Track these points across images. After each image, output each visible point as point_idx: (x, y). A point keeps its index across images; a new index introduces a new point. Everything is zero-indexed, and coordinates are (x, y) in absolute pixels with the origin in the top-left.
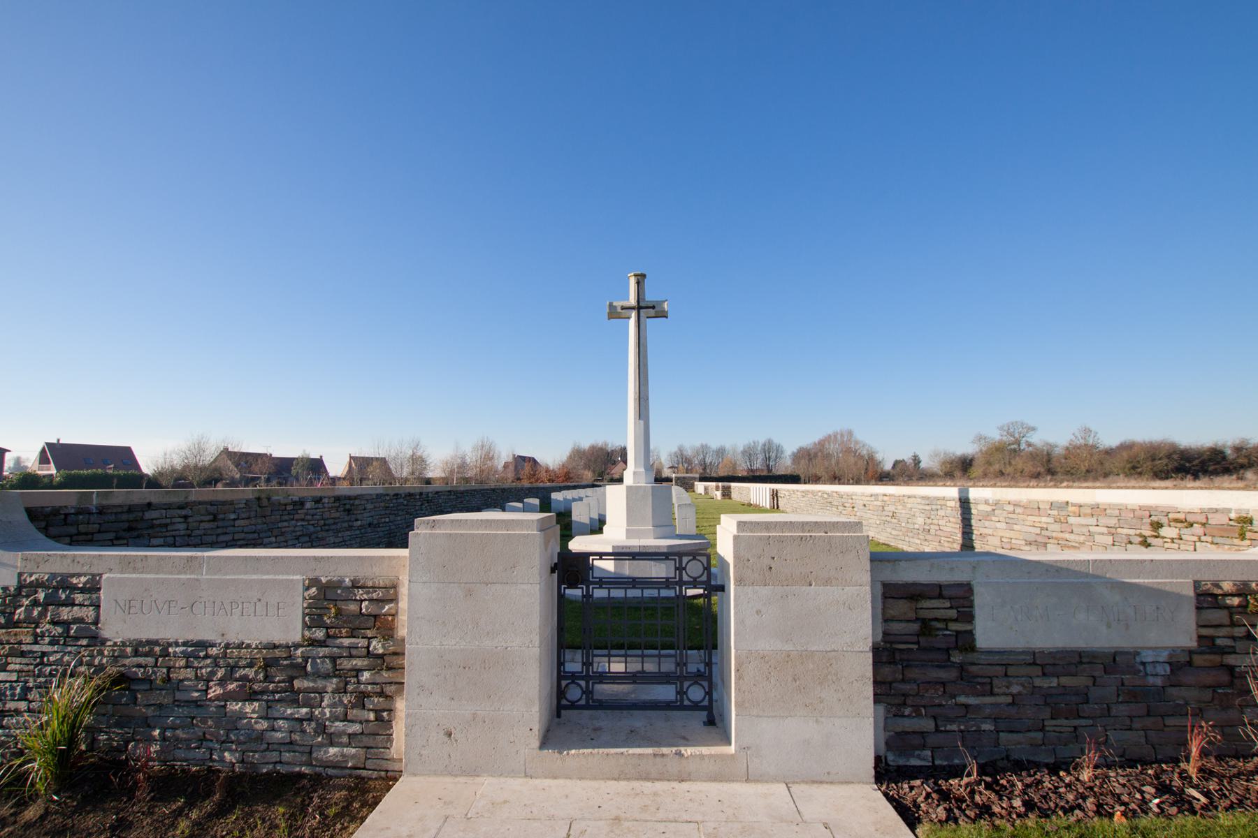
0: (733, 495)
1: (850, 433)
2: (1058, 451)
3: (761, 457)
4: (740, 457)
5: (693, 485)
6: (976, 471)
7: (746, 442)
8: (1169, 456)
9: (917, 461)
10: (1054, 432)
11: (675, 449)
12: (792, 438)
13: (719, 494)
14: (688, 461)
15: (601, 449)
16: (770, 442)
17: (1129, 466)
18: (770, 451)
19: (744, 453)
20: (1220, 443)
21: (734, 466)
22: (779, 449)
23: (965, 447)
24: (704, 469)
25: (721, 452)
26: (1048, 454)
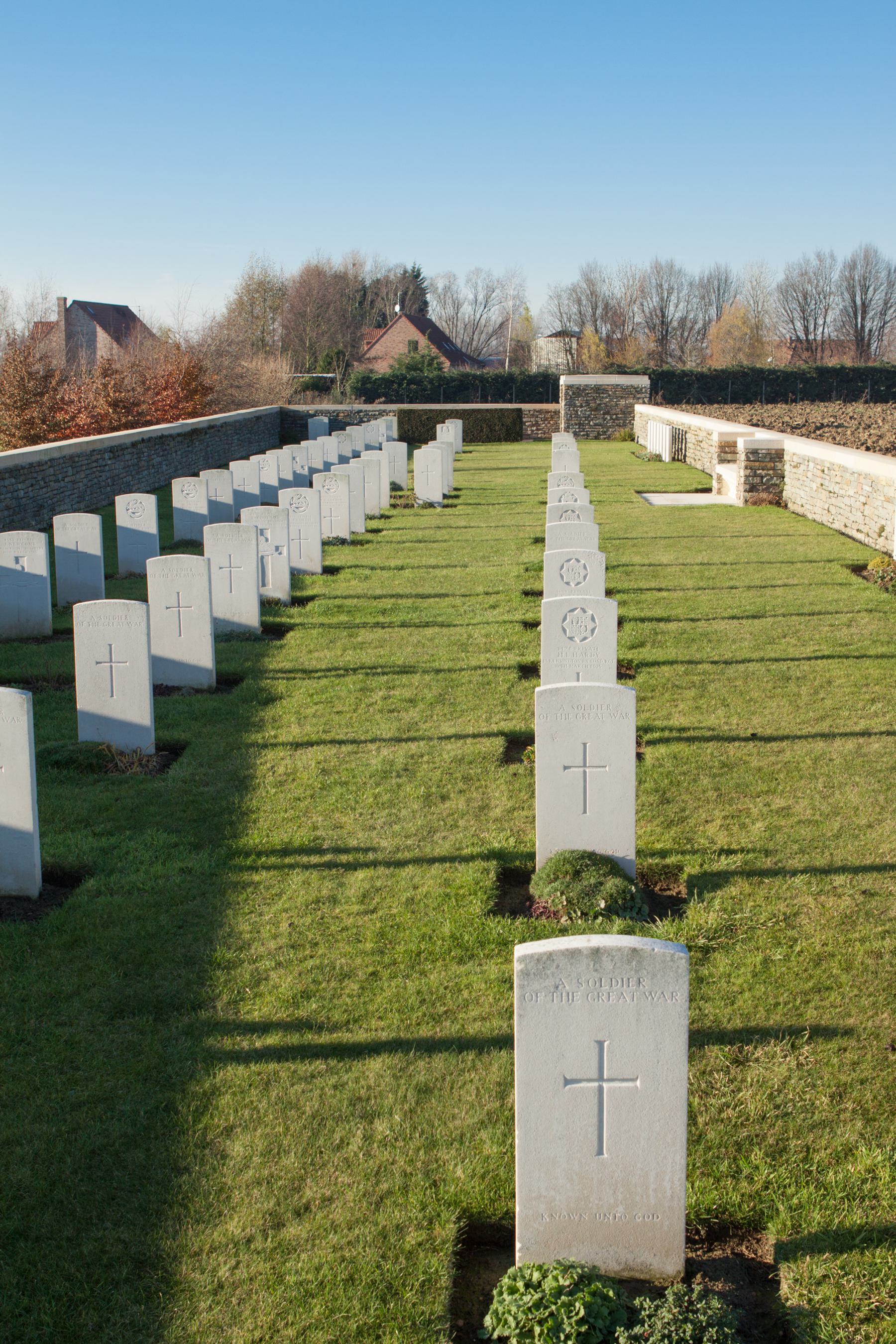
0: (791, 491)
3: (838, 304)
4: (773, 303)
5: (629, 413)
11: (571, 277)
13: (731, 482)
14: (613, 314)
15: (340, 278)
16: (869, 257)
19: (786, 290)
21: (755, 337)
24: (663, 340)
25: (715, 288)
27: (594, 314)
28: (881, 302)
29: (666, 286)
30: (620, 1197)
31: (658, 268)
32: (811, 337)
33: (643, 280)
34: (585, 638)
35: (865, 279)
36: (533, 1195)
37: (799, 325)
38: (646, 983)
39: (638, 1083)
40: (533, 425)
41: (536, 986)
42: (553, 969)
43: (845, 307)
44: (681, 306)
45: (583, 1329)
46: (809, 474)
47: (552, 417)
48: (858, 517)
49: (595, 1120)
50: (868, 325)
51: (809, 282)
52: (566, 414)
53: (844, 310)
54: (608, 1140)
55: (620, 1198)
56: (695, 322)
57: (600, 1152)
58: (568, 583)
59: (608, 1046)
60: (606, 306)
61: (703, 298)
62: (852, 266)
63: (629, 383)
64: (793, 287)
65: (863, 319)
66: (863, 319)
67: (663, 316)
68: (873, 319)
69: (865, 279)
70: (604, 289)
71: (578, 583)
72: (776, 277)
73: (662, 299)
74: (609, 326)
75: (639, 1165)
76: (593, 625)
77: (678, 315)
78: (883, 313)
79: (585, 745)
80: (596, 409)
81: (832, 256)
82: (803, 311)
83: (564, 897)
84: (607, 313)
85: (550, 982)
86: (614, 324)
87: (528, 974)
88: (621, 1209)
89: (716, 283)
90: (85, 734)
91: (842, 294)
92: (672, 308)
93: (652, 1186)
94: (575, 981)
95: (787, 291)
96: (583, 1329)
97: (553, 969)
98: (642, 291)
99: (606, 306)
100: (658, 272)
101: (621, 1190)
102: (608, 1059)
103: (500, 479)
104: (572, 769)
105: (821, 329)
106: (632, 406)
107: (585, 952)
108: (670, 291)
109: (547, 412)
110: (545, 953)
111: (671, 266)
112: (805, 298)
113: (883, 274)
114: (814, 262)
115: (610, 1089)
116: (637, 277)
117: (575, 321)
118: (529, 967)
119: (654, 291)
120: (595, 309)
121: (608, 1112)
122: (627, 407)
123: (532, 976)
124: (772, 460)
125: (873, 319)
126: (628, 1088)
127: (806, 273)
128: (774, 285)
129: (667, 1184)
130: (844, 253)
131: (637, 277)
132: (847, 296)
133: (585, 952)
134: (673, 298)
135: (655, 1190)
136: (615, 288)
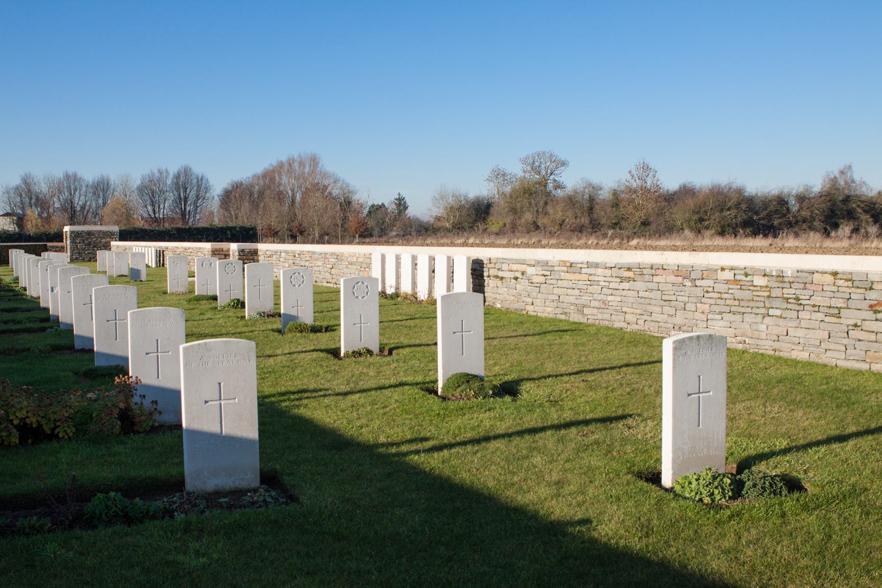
1: (314, 161)
2: (605, 195)
3: (171, 197)
6: (494, 223)
7: (146, 171)
8: (737, 206)
9: (401, 204)
10: (596, 166)
12: (224, 166)
14: (41, 203)
16: (187, 172)
17: (696, 217)
18: (187, 186)
19: (141, 190)
20: (786, 191)
22: (202, 185)
23: (479, 187)
26: (591, 200)
29: (73, 187)
31: (67, 177)
32: (157, 215)
37: (150, 208)
46: (282, 260)
48: (328, 276)
50: (188, 209)
53: (174, 201)
60: (37, 199)
61: (94, 193)
62: (177, 177)
64: (146, 187)
65: (185, 205)
66: (185, 205)
70: (36, 189)
77: (80, 203)
78: (195, 203)
80: (89, 244)
81: (167, 171)
85: (683, 351)
86: (42, 208)
90: (98, 363)
92: (77, 200)
99: (37, 199)
106: (109, 242)
108: (75, 190)
111: (75, 176)
113: (195, 181)
114: (157, 174)
120: (31, 199)
122: (106, 243)
124: (252, 255)
128: (135, 187)
130: (173, 170)
132: (176, 193)
136: (43, 188)
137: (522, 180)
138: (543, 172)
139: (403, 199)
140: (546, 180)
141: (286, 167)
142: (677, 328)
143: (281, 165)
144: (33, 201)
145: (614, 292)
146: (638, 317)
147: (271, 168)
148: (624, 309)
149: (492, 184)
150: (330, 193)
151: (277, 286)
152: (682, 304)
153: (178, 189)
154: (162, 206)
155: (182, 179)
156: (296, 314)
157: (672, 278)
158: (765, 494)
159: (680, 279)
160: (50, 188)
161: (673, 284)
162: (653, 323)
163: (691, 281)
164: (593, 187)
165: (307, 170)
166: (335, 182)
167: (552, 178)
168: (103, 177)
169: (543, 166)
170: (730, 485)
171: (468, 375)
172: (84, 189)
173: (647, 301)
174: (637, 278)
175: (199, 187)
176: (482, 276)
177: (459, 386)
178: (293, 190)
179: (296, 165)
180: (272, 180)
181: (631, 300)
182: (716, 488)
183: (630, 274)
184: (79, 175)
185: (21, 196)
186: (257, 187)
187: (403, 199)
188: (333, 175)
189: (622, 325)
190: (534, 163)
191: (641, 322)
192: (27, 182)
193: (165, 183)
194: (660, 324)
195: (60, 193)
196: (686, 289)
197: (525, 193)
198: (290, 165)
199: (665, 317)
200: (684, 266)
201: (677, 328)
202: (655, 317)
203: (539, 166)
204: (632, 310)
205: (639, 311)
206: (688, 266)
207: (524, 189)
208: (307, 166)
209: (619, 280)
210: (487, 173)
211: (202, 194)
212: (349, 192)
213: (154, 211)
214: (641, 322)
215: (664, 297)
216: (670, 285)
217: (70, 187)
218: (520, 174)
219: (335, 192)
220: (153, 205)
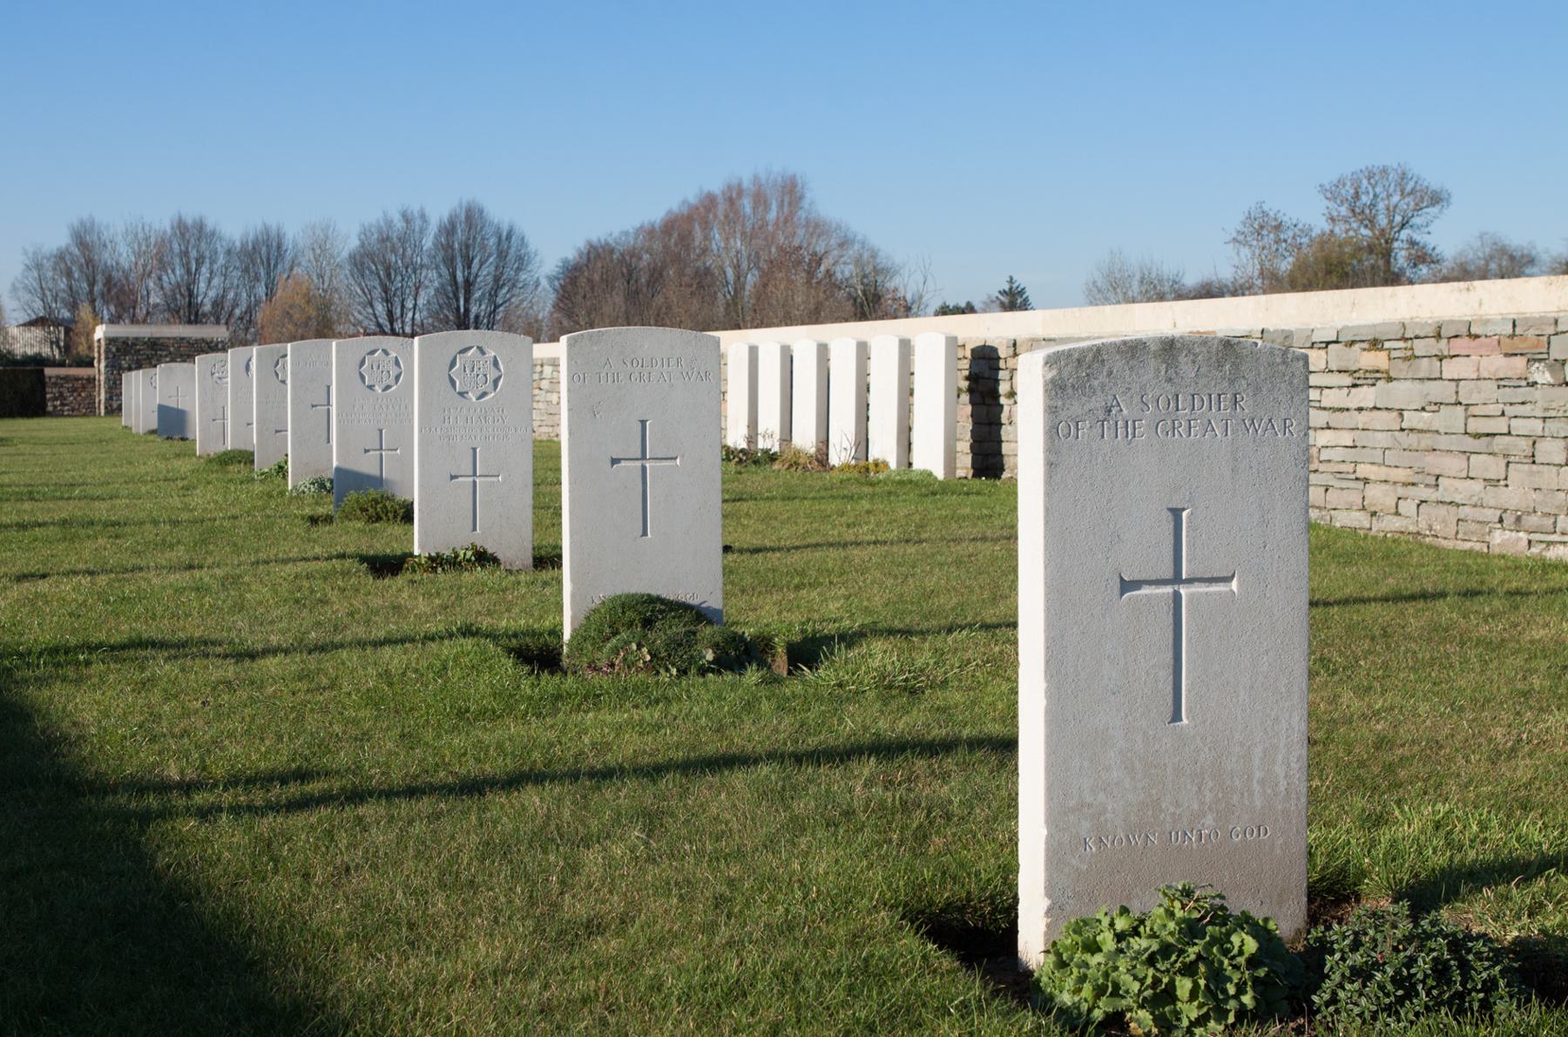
1: (791, 191)
3: (433, 280)
4: (344, 279)
7: (373, 216)
16: (472, 217)
19: (360, 262)
27: (91, 292)
28: (490, 279)
29: (193, 254)
30: (1209, 797)
31: (181, 228)
33: (163, 243)
34: (484, 394)
35: (467, 247)
36: (1072, 803)
37: (380, 308)
38: (1246, 403)
39: (1234, 585)
40: (55, 399)
41: (1076, 409)
42: (1102, 378)
43: (442, 286)
44: (215, 282)
45: (1262, 972)
47: (84, 387)
49: (1169, 656)
50: (474, 310)
51: (394, 250)
52: (107, 379)
54: (1189, 691)
55: (1208, 800)
56: (235, 305)
57: (1176, 716)
58: (371, 387)
59: (1189, 517)
60: (109, 281)
61: (246, 270)
62: (449, 230)
63: (199, 336)
64: (371, 256)
66: (467, 301)
67: (191, 295)
68: (480, 301)
69: (467, 247)
70: (106, 257)
71: (388, 387)
72: (348, 242)
73: (188, 272)
74: (112, 308)
75: (1237, 736)
76: (497, 374)
77: (212, 294)
78: (493, 294)
79: (643, 423)
81: (423, 216)
82: (385, 290)
83: (645, 650)
84: (109, 291)
85: (1098, 402)
87: (1063, 388)
88: (1209, 820)
89: (264, 250)
91: (437, 268)
92: (202, 285)
93: (1258, 775)
94: (1137, 399)
95: (362, 264)
96: (1262, 972)
97: (1102, 378)
98: (161, 260)
99: (109, 281)
100: (183, 235)
101: (1210, 784)
102: (1188, 543)
103: (42, 434)
104: (623, 463)
105: (410, 315)
107: (1153, 348)
109: (77, 379)
110: (1090, 349)
111: (200, 227)
112: (389, 275)
113: (492, 241)
114: (399, 224)
115: (1191, 597)
116: (152, 240)
117: (63, 300)
118: (1065, 375)
119: (177, 260)
120: (92, 284)
121: (1189, 640)
123: (1070, 391)
125: (480, 301)
126: (1220, 593)
127: (388, 238)
128: (345, 254)
129: (1279, 770)
130: (439, 210)
131: (152, 240)
132: (444, 271)
133: (1153, 348)
134: (204, 270)
135: (1262, 782)
136: (121, 255)
137: (1324, 241)
138: (1382, 221)
139: (1021, 292)
140: (1389, 241)
141: (722, 208)
142: (1509, 519)
143: (710, 202)
144: (98, 288)
145: (1336, 419)
146: (1401, 491)
147: (685, 211)
148: (1363, 470)
149: (1245, 251)
150: (829, 274)
151: (545, 458)
152: (1524, 444)
153: (450, 262)
154: (409, 304)
155: (460, 235)
156: (375, 472)
157: (1497, 364)
158: (1407, 1011)
159: (1520, 362)
160: (138, 255)
161: (1501, 382)
162: (1443, 510)
163: (1551, 368)
164: (1512, 258)
165: (772, 215)
166: (841, 245)
167: (1404, 234)
168: (267, 230)
169: (1381, 206)
170: (1253, 962)
171: (652, 600)
172: (221, 260)
173: (1427, 441)
174: (1399, 369)
175: (502, 255)
176: (995, 395)
177: (615, 633)
178: (737, 267)
179: (747, 205)
180: (685, 239)
181: (1382, 439)
182: (1189, 970)
183: (1378, 360)
184: (210, 224)
185: (69, 274)
186: (646, 257)
187: (1021, 292)
188: (839, 227)
189: (1358, 519)
190: (1357, 196)
191: (1408, 507)
192: (85, 241)
193: (418, 247)
194: (1465, 512)
195: (163, 268)
196: (1536, 394)
197: (1329, 272)
198: (731, 201)
199: (1477, 486)
200: (1531, 322)
201: (1509, 519)
202: (1448, 489)
203: (1373, 205)
204: (1382, 472)
205: (1401, 475)
206: (1542, 321)
207: (1327, 260)
208: (774, 207)
209: (1348, 380)
210: (1234, 222)
211: (509, 273)
212: (876, 271)
213: (390, 314)
214: (1408, 507)
215: (1476, 426)
216: (1493, 385)
217: (186, 253)
218: (1320, 225)
219: (845, 271)
220: (387, 300)
